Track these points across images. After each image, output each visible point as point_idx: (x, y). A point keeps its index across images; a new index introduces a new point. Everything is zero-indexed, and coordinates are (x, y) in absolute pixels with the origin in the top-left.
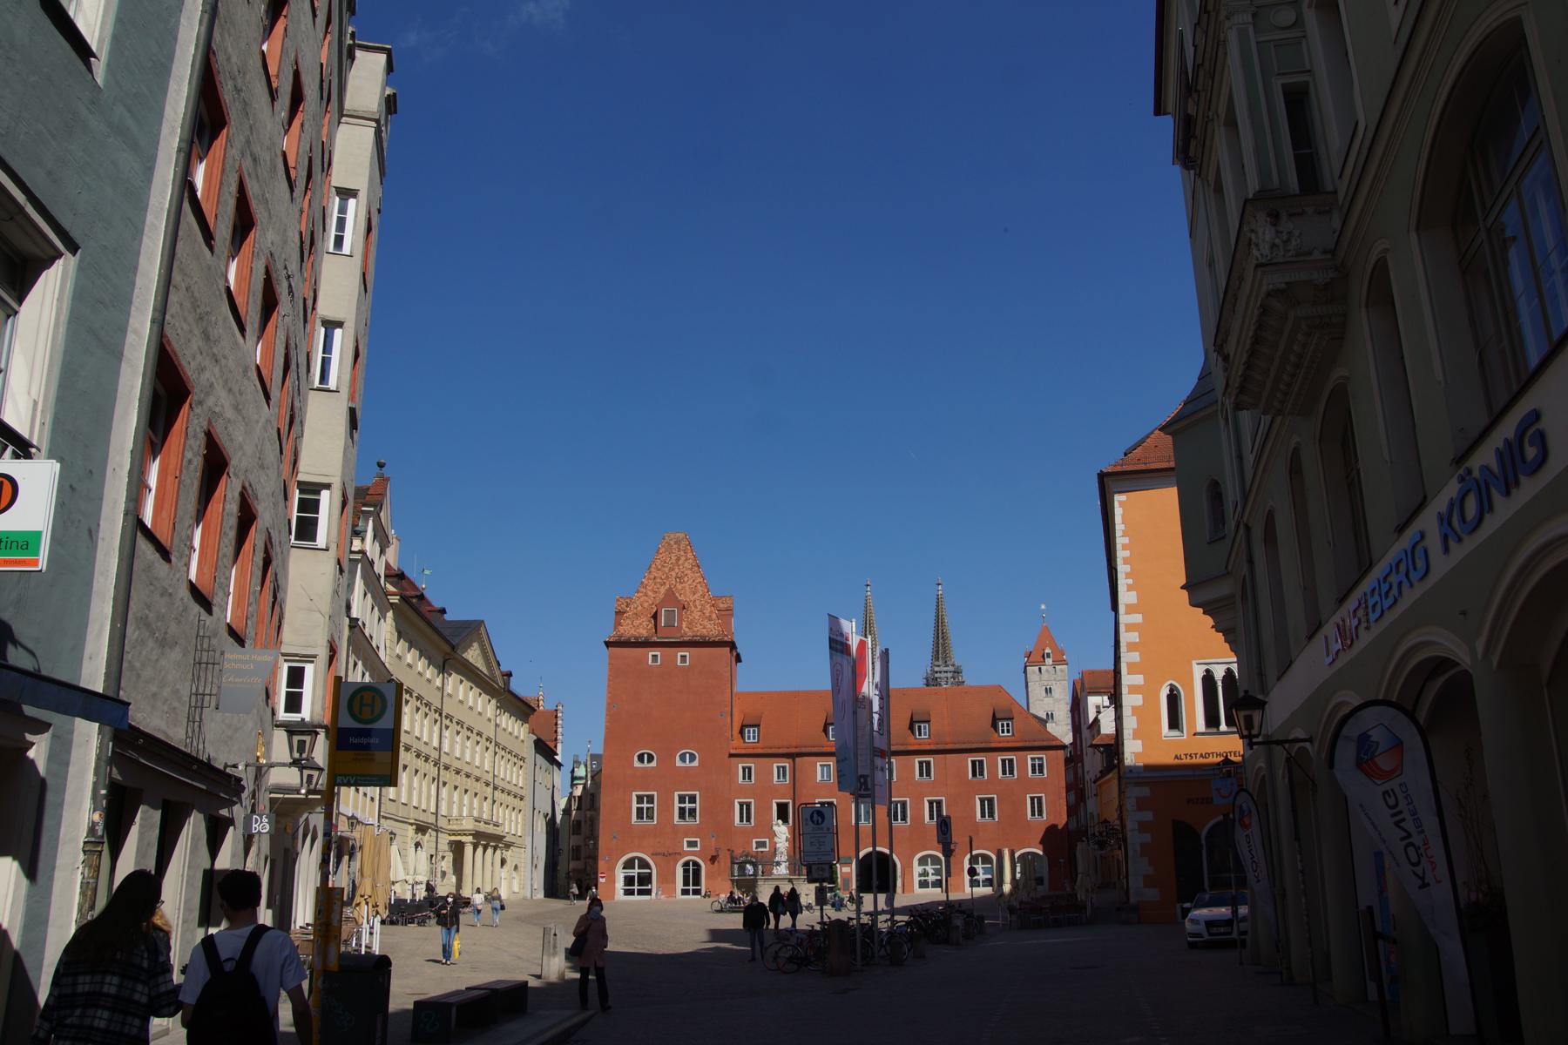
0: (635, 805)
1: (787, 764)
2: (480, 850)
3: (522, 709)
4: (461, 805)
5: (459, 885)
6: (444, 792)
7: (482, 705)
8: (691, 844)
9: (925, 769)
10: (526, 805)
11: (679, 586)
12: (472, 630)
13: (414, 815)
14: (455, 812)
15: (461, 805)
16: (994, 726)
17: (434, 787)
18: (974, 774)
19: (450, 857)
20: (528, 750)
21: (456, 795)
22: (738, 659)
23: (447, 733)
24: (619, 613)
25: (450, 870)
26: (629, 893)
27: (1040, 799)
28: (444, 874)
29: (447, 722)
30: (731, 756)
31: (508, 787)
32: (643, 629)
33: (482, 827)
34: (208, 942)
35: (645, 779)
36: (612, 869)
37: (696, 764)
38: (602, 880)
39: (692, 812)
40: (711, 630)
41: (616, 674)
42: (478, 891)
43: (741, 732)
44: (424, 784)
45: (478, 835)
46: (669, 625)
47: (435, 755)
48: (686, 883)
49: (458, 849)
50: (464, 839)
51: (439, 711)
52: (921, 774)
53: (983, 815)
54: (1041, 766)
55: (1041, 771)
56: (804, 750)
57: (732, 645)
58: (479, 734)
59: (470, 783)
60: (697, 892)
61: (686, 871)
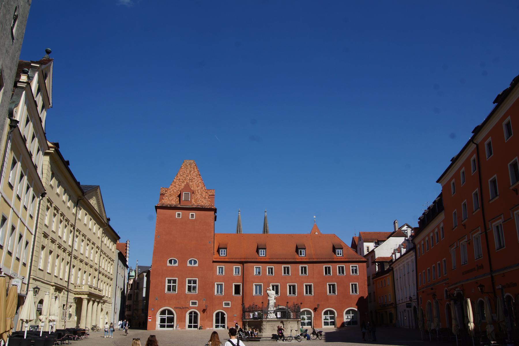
0: (167, 284)
1: (240, 266)
2: (91, 303)
3: (114, 237)
4: (82, 279)
5: (78, 322)
6: (73, 271)
7: (97, 231)
8: (194, 303)
9: (304, 270)
10: (113, 283)
11: (191, 183)
12: (94, 190)
13: (54, 281)
14: (79, 282)
15: (82, 279)
16: (257, 251)
17: (67, 267)
18: (326, 273)
19: (74, 306)
20: (115, 257)
21: (80, 273)
23: (77, 240)
25: (74, 314)
26: (162, 326)
27: (356, 285)
28: (70, 315)
29: (78, 233)
30: (214, 262)
31: (105, 273)
32: (173, 201)
33: (93, 291)
34: (260, 331)
35: (172, 272)
36: (155, 315)
37: (197, 265)
38: (150, 320)
39: (194, 288)
40: (205, 203)
41: (160, 222)
42: (107, 323)
43: (218, 251)
44: (62, 264)
45: (90, 295)
47: (69, 249)
48: (190, 322)
49: (79, 302)
50: (82, 296)
51: (73, 226)
52: (302, 273)
53: (330, 292)
54: (356, 270)
55: (356, 272)
56: (248, 260)
58: (93, 244)
59: (87, 268)
60: (196, 327)
61: (190, 317)
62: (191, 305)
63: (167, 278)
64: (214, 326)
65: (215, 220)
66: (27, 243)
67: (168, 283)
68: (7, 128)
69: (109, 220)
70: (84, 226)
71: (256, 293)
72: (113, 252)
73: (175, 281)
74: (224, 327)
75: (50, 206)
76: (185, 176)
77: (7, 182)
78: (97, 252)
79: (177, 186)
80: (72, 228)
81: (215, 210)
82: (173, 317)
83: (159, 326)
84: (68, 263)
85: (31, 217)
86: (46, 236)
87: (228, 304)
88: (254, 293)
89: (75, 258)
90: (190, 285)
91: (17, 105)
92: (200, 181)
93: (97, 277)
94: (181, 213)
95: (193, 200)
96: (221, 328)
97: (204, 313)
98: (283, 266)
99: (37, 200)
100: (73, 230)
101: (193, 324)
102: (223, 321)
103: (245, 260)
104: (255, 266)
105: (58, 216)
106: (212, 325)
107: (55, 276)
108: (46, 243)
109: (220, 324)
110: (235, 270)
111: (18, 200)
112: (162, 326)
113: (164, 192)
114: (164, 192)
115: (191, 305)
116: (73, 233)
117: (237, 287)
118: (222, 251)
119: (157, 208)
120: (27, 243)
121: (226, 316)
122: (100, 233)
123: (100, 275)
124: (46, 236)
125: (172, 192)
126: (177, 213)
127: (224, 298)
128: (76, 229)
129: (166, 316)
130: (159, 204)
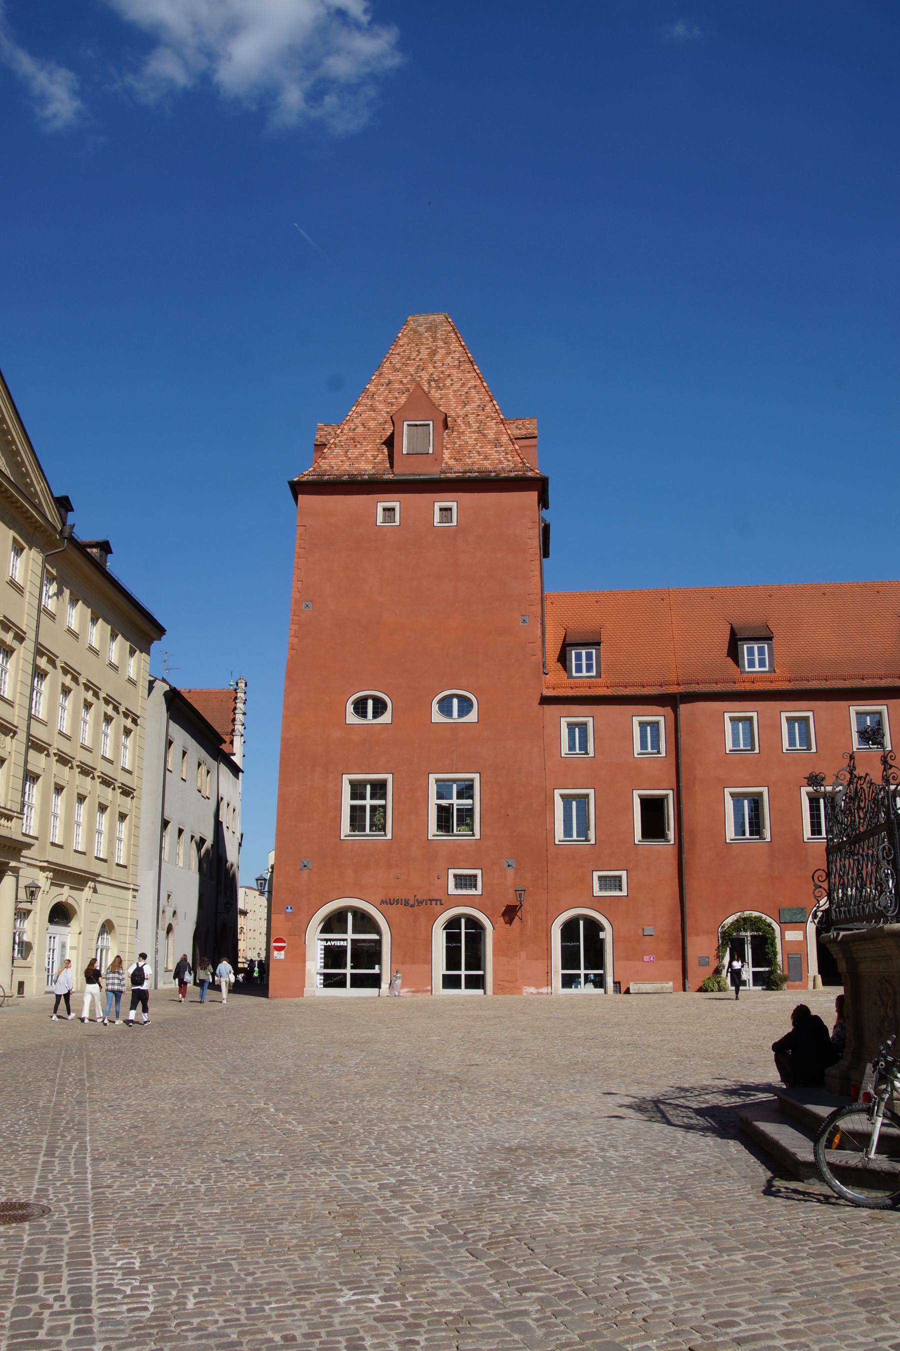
1: (660, 717)
3: (140, 627)
8: (465, 881)
16: (734, 653)
26: (331, 981)
30: (545, 701)
32: (367, 461)
37: (472, 717)
39: (466, 815)
40: (500, 460)
43: (563, 659)
48: (452, 961)
56: (693, 688)
60: (476, 982)
61: (452, 938)
62: (452, 890)
63: (346, 778)
64: (557, 981)
65: (546, 553)
67: (353, 797)
69: (64, 504)
73: (379, 789)
74: (599, 982)
76: (412, 370)
79: (380, 406)
81: (540, 486)
82: (379, 942)
83: (319, 980)
87: (616, 882)
90: (444, 802)
92: (473, 383)
94: (396, 505)
95: (446, 454)
96: (590, 989)
97: (510, 922)
98: (854, 709)
101: (463, 972)
102: (596, 958)
103: (682, 689)
104: (729, 712)
106: (549, 973)
109: (582, 972)
110: (639, 732)
112: (331, 981)
115: (452, 890)
117: (653, 810)
118: (579, 657)
119: (298, 488)
121: (607, 935)
126: (380, 506)
127: (597, 857)
129: (348, 937)
130: (307, 474)
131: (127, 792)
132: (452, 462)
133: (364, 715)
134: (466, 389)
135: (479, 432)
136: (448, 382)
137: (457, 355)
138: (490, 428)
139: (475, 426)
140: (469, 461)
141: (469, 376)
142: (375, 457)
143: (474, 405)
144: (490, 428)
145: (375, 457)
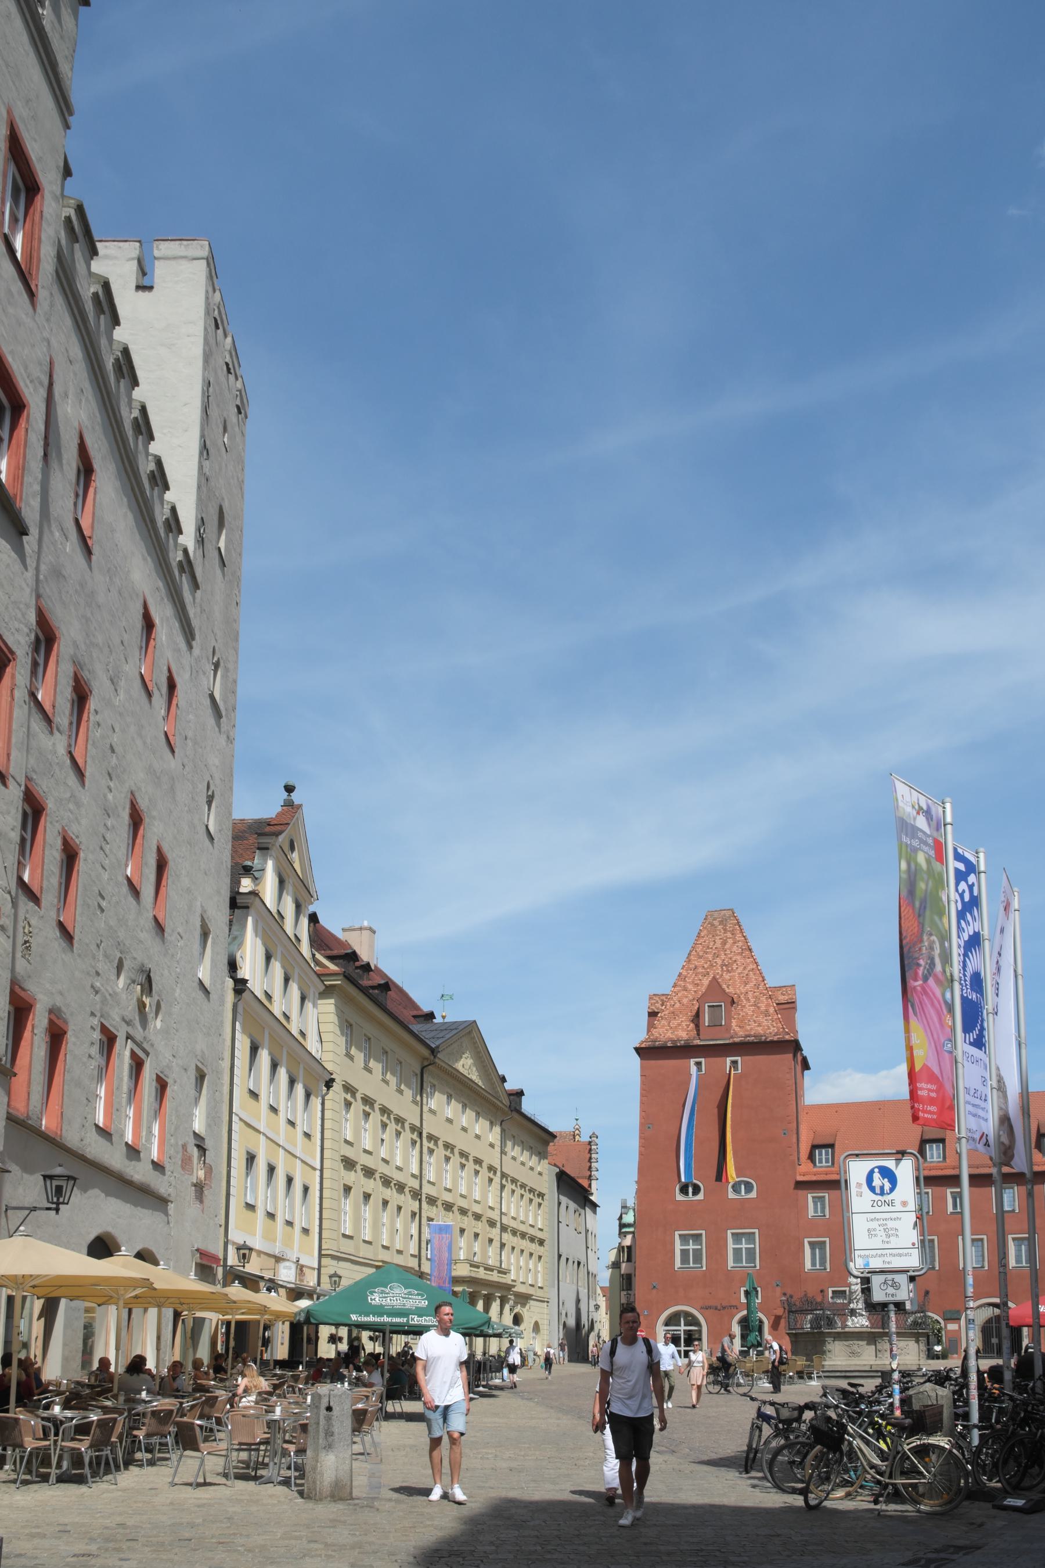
7: (482, 1134)
10: (548, 1251)
11: (727, 976)
22: (806, 1066)
24: (652, 1014)
31: (522, 1228)
37: (753, 1195)
40: (768, 1028)
43: (811, 1157)
46: (715, 1024)
57: (795, 1046)
66: (306, 1189)
68: (230, 997)
70: (448, 1124)
71: (813, 1264)
72: (540, 1174)
75: (352, 1100)
76: (710, 957)
77: (247, 1090)
78: (491, 1180)
79: (690, 987)
80: (415, 1136)
84: (414, 1214)
85: (307, 1135)
86: (349, 1164)
88: (808, 1265)
89: (432, 1201)
91: (241, 945)
92: (751, 966)
93: (496, 1239)
95: (734, 1023)
99: (316, 1102)
100: (418, 1140)
105: (376, 1117)
107: (384, 1247)
108: (353, 1179)
111: (273, 1115)
113: (658, 1005)
114: (658, 1005)
116: (418, 1144)
120: (306, 1189)
122: (494, 1135)
123: (505, 1236)
124: (349, 1164)
125: (678, 1005)
128: (424, 1135)
131: (541, 1242)
132: (737, 1029)
133: (687, 1194)
134: (746, 972)
135: (755, 1005)
136: (735, 966)
137: (740, 944)
138: (762, 1002)
139: (752, 1000)
140: (748, 1028)
141: (748, 960)
142: (688, 1026)
143: (752, 984)
144: (762, 1002)
145: (688, 1026)
